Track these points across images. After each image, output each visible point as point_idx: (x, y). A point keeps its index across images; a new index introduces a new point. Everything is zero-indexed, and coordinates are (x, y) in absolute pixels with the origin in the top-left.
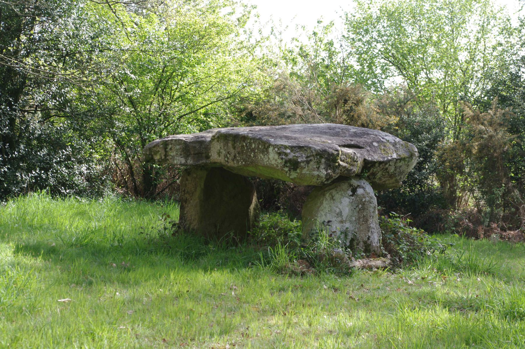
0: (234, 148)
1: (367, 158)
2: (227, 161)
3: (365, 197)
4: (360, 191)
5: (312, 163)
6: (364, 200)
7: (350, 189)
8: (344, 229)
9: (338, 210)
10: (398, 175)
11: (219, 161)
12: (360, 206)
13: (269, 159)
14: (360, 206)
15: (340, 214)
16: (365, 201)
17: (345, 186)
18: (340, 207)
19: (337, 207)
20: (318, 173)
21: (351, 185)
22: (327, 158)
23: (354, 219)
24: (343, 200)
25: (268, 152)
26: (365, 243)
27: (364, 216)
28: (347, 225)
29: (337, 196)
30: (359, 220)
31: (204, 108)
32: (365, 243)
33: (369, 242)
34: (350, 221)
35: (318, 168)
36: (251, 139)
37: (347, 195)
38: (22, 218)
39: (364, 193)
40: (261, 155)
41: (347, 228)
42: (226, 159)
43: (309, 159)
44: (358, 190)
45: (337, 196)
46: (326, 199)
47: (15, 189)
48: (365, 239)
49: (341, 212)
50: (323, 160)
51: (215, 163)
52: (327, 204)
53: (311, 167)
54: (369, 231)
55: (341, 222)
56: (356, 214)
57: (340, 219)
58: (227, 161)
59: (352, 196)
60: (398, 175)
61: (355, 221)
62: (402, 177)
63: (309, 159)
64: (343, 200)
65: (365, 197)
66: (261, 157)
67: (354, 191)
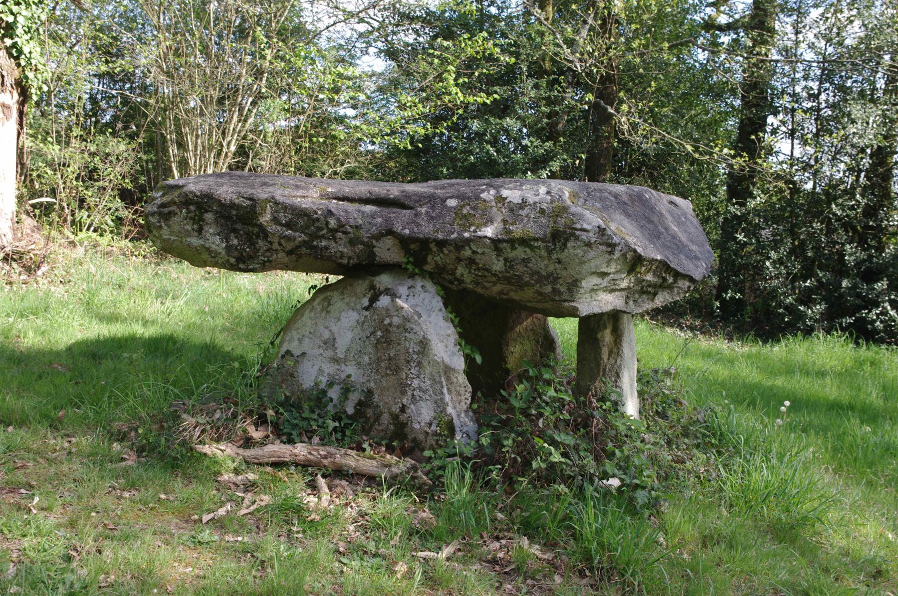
3: (390, 316)
5: (176, 219)
6: (387, 321)
7: (369, 296)
8: (343, 376)
9: (326, 334)
12: (379, 333)
14: (379, 333)
15: (330, 343)
16: (390, 324)
18: (335, 329)
19: (327, 328)
20: (201, 242)
21: (372, 287)
22: (217, 212)
23: (366, 359)
26: (395, 417)
27: (390, 359)
28: (350, 369)
30: (378, 364)
31: (795, 146)
32: (395, 417)
33: (403, 417)
34: (359, 363)
35: (200, 231)
39: (391, 307)
41: (349, 376)
43: (166, 210)
48: (396, 409)
49: (334, 339)
50: (209, 217)
52: (311, 318)
53: (176, 228)
54: (403, 393)
55: (335, 360)
56: (369, 349)
57: (330, 353)
59: (366, 309)
61: (370, 364)
63: (166, 210)
65: (390, 316)
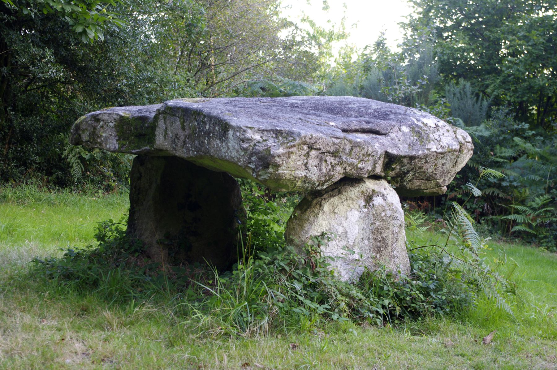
0: (183, 129)
1: (390, 150)
2: (175, 149)
4: (378, 201)
5: (293, 157)
10: (441, 176)
11: (164, 148)
13: (228, 148)
17: (354, 192)
18: (345, 225)
24: (350, 214)
25: (227, 138)
29: (342, 208)
36: (205, 116)
37: (357, 206)
38: (396, 174)
40: (218, 141)
42: (174, 145)
44: (374, 198)
45: (342, 208)
46: (324, 212)
47: (304, 93)
51: (161, 150)
58: (175, 149)
60: (441, 176)
62: (447, 179)
64: (350, 214)
66: (217, 144)
67: (369, 199)
